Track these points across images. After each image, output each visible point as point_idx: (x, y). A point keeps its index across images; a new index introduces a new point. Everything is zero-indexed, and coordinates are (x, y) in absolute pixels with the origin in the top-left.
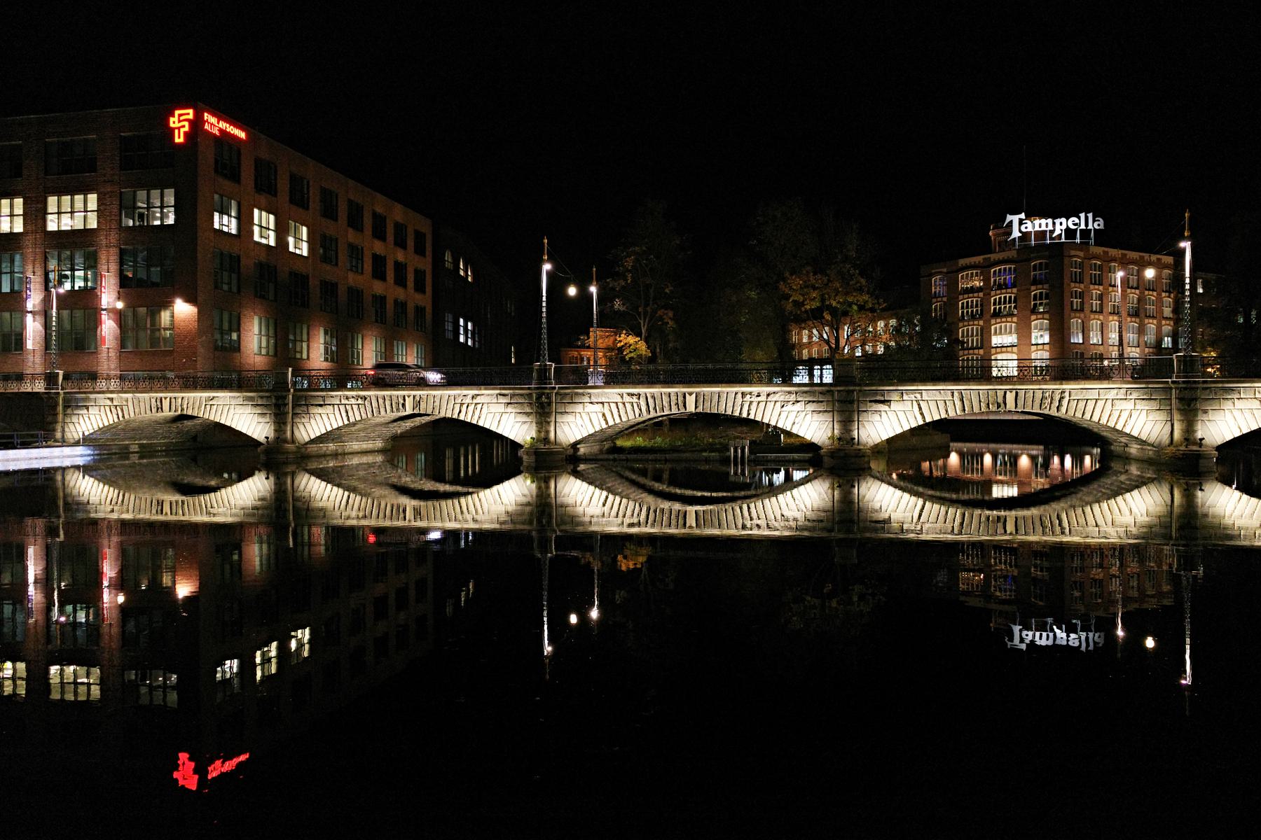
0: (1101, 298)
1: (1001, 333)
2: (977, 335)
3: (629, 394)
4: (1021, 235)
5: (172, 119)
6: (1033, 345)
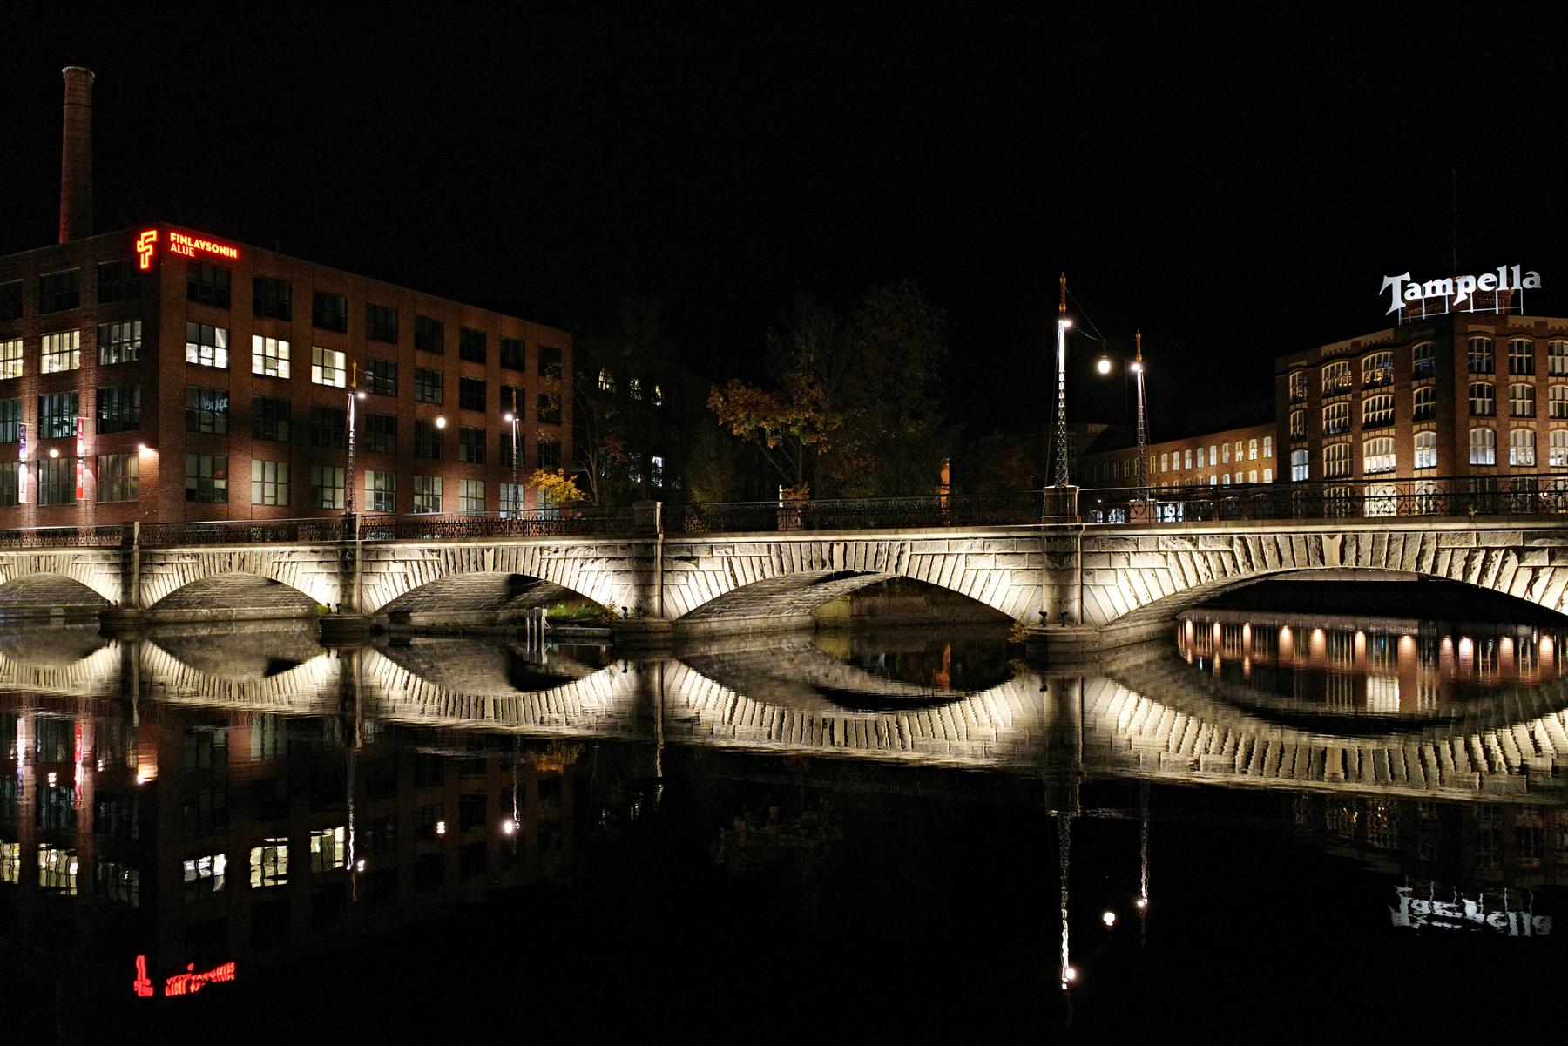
0: (1532, 394)
1: (1375, 454)
2: (1345, 457)
3: (429, 550)
4: (1404, 305)
5: (139, 243)
6: (1416, 469)
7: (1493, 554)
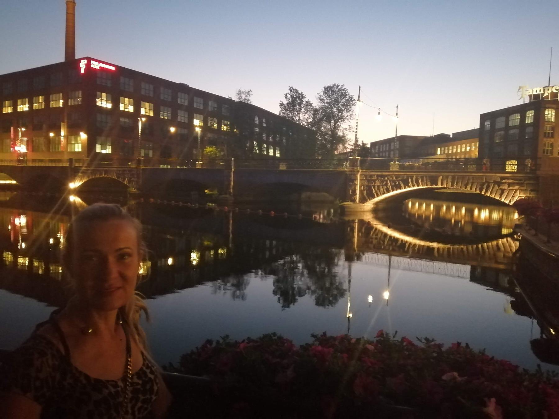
7: (490, 184)
